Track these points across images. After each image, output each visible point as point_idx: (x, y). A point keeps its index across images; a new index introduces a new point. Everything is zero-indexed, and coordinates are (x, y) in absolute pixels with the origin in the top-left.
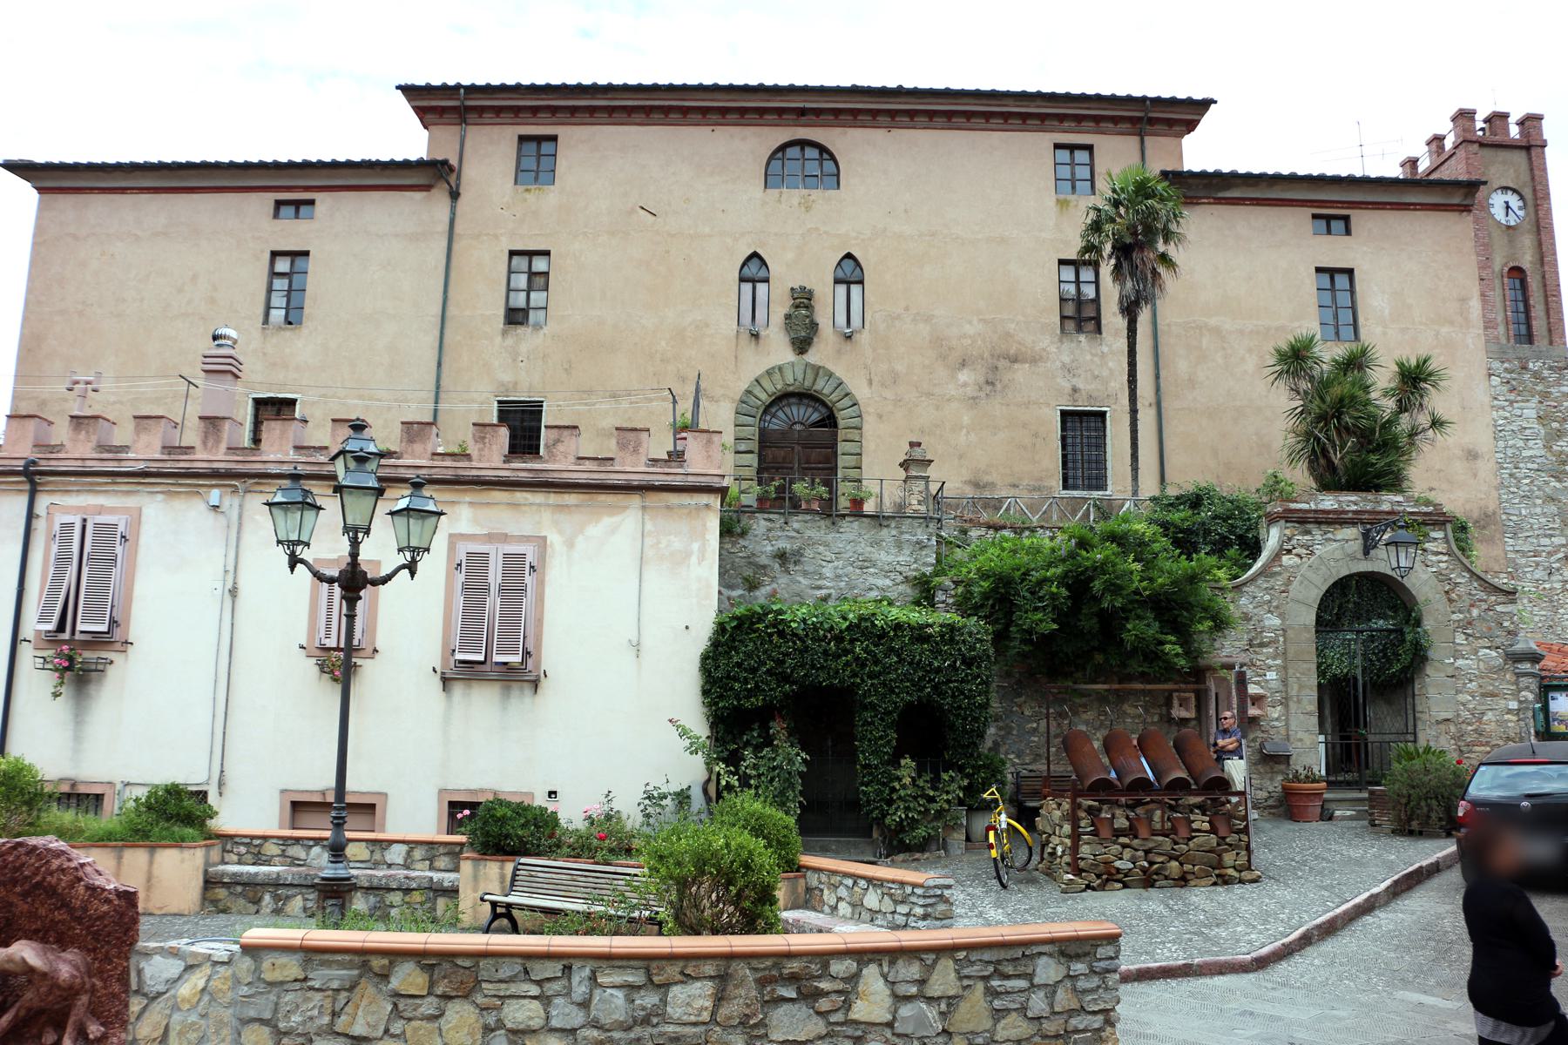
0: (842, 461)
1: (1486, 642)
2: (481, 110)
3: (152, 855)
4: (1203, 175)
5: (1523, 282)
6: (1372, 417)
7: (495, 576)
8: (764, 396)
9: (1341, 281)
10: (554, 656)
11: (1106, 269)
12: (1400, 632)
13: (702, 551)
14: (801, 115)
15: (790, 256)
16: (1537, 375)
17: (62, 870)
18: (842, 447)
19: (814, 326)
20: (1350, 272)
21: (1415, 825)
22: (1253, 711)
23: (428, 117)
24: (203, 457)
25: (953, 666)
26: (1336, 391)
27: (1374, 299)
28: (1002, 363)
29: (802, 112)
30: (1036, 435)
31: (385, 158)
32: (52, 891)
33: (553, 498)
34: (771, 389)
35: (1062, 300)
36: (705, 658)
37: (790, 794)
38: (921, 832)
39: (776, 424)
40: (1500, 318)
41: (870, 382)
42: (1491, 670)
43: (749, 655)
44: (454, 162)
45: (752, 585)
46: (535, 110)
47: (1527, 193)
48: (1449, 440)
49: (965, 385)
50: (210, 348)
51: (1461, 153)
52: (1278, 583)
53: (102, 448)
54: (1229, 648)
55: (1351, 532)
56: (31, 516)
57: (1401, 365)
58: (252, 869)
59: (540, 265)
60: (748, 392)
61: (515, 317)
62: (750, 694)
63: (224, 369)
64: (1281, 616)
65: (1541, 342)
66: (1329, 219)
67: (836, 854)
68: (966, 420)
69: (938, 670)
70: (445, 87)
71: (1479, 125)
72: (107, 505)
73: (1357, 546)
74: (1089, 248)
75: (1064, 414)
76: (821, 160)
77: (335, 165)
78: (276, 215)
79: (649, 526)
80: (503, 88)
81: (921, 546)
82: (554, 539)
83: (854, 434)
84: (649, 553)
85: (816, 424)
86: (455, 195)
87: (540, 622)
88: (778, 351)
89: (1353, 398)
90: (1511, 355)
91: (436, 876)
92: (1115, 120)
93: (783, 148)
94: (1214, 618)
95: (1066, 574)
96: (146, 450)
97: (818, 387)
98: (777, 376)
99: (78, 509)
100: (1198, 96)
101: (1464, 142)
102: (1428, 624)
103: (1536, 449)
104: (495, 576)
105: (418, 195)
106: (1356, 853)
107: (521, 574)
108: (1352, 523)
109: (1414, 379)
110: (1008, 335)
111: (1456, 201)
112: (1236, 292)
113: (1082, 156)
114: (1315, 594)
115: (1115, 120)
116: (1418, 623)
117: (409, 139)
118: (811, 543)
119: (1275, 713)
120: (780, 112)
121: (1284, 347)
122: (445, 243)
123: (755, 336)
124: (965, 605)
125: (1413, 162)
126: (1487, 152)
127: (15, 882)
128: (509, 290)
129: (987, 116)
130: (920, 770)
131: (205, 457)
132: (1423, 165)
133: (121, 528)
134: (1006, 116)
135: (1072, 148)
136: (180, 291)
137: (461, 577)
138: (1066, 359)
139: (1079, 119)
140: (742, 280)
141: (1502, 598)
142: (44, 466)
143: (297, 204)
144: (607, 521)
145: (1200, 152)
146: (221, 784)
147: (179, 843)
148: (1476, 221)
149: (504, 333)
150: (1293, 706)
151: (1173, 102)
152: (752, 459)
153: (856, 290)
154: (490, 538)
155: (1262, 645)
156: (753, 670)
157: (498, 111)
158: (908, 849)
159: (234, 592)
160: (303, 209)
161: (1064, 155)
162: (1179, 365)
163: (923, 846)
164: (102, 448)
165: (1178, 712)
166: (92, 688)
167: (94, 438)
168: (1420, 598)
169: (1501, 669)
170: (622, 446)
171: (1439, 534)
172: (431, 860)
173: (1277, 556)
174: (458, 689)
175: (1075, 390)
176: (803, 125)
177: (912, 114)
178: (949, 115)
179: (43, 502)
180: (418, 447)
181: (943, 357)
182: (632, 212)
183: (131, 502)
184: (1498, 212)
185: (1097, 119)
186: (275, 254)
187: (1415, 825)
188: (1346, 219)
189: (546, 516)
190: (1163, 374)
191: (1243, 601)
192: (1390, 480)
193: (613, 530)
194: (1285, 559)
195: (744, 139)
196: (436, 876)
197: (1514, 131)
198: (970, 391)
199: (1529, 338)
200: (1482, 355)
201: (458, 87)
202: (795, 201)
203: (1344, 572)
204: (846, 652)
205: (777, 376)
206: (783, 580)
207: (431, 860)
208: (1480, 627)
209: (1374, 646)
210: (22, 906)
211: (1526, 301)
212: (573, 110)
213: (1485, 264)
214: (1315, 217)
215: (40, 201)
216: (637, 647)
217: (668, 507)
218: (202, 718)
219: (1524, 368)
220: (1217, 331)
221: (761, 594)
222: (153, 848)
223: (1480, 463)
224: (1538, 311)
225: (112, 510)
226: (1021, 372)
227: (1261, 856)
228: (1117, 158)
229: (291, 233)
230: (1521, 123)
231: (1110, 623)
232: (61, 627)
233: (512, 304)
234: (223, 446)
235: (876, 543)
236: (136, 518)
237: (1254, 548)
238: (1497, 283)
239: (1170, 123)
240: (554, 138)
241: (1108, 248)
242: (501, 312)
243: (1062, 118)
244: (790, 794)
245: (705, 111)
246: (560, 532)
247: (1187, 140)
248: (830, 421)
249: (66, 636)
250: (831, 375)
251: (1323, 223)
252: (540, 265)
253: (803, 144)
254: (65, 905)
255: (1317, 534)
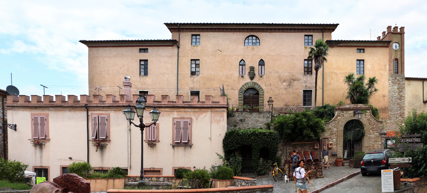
0: (260, 101)
1: (376, 132)
2: (183, 29)
3: (114, 180)
4: (335, 41)
5: (398, 61)
6: (363, 89)
7: (182, 125)
8: (244, 89)
9: (362, 62)
10: (194, 141)
11: (313, 61)
12: (360, 130)
13: (223, 120)
14: (252, 30)
15: (250, 60)
16: (398, 80)
17: (76, 179)
18: (260, 99)
19: (254, 74)
20: (363, 60)
21: (357, 166)
22: (330, 147)
23: (172, 30)
24: (121, 103)
25: (270, 140)
26: (356, 84)
27: (368, 66)
28: (292, 81)
29: (252, 29)
30: (298, 95)
31: (162, 39)
32: (75, 183)
33: (193, 110)
34: (246, 87)
35: (304, 68)
36: (224, 140)
37: (239, 166)
38: (264, 172)
39: (247, 94)
40: (392, 69)
41: (266, 86)
42: (376, 137)
43: (232, 140)
44: (178, 40)
45: (235, 126)
46: (195, 29)
47: (400, 43)
48: (377, 94)
49: (284, 86)
50: (124, 80)
51: (388, 35)
52: (337, 122)
53: (100, 101)
54: (327, 135)
55: (352, 112)
56: (88, 116)
57: (370, 79)
58: (134, 183)
59: (198, 62)
60: (241, 88)
61: (193, 73)
62: (232, 147)
63: (128, 85)
64: (337, 128)
65: (400, 73)
66: (360, 49)
67: (246, 176)
68: (284, 93)
69: (268, 141)
70: (174, 23)
71: (392, 29)
72: (103, 113)
73: (352, 115)
74: (309, 57)
75: (304, 91)
76: (256, 39)
77: (151, 41)
78: (140, 52)
79: (212, 115)
80: (187, 24)
81: (268, 117)
82: (194, 118)
83: (262, 96)
84: (213, 120)
85: (255, 94)
86: (178, 47)
87: (191, 134)
88: (247, 79)
89: (359, 85)
90: (393, 76)
91: (168, 183)
92: (317, 29)
93: (248, 37)
94: (322, 130)
95: (293, 122)
96: (109, 102)
97: (255, 87)
98: (247, 85)
99: (97, 114)
100: (335, 23)
101: (389, 33)
102: (365, 129)
103: (396, 94)
104: (182, 125)
105: (170, 48)
106: (344, 172)
107: (188, 125)
108: (352, 110)
109: (372, 81)
110: (293, 75)
111: (386, 45)
112: (339, 65)
113: (310, 38)
114: (344, 124)
115: (317, 29)
116: (363, 128)
117: (168, 35)
118: (247, 117)
119: (335, 147)
120: (248, 29)
121: (347, 76)
122: (177, 58)
123: (243, 77)
124: (275, 129)
125: (379, 37)
126: (393, 35)
127: (68, 182)
128: (191, 68)
129: (291, 29)
130: (264, 160)
131: (121, 103)
132: (381, 38)
133: (106, 118)
134: (295, 29)
135: (308, 36)
136: (121, 68)
137: (175, 126)
138: (305, 80)
139: (310, 29)
140: (240, 65)
141: (380, 123)
142: (89, 105)
143: (144, 49)
144: (204, 114)
145: (335, 36)
146: (130, 167)
147: (119, 178)
148: (389, 49)
149: (191, 77)
150: (338, 145)
151: (330, 25)
152: (242, 102)
153: (263, 67)
154: (181, 118)
155: (333, 134)
156: (232, 142)
157: (187, 29)
158: (261, 175)
159: (130, 130)
160: (146, 50)
161: (307, 37)
162: (328, 80)
163: (264, 174)
164: (100, 101)
165: (316, 147)
166: (104, 150)
167: (98, 99)
168: (364, 124)
169: (378, 136)
170: (206, 99)
171: (369, 112)
172: (168, 180)
173: (337, 117)
174: (176, 148)
175: (306, 86)
176: (252, 30)
177: (275, 29)
178: (283, 29)
179: (90, 113)
180: (165, 100)
181: (280, 80)
182: (216, 51)
183: (107, 112)
184: (394, 47)
185: (314, 29)
186: (140, 60)
187: (357, 166)
188: (364, 49)
189: (192, 113)
190: (324, 82)
191: (330, 126)
192: (365, 101)
193: (205, 116)
194: (338, 117)
195: (240, 35)
196: (168, 183)
197: (399, 31)
198: (285, 87)
199: (398, 73)
200: (388, 76)
201: (178, 23)
202: (251, 48)
203: (350, 120)
204: (250, 138)
205: (247, 85)
206: (241, 125)
207: (168, 180)
208: (375, 129)
209: (354, 134)
210: (70, 186)
211: (398, 65)
212: (203, 29)
213: (390, 58)
214: (357, 49)
215: (89, 51)
216: (210, 139)
217: (216, 111)
218: (126, 155)
219: (396, 79)
220: (336, 73)
221: (237, 127)
222: (114, 179)
223: (385, 98)
224: (400, 67)
225: (104, 114)
226: (296, 83)
227: (324, 173)
228: (317, 37)
229: (144, 56)
230: (400, 29)
231: (301, 130)
232: (96, 137)
233: (192, 71)
234: (125, 101)
235: (259, 117)
236: (109, 116)
237: (334, 115)
238: (392, 62)
239: (329, 30)
240: (199, 35)
241: (313, 57)
242: (190, 72)
243: (306, 29)
244: (239, 166)
245: (231, 29)
246: (195, 117)
247: (333, 33)
248: (258, 94)
249: (98, 139)
250: (258, 84)
251: (359, 50)
252: (198, 62)
253: (252, 36)
254: (77, 186)
255: (345, 112)
